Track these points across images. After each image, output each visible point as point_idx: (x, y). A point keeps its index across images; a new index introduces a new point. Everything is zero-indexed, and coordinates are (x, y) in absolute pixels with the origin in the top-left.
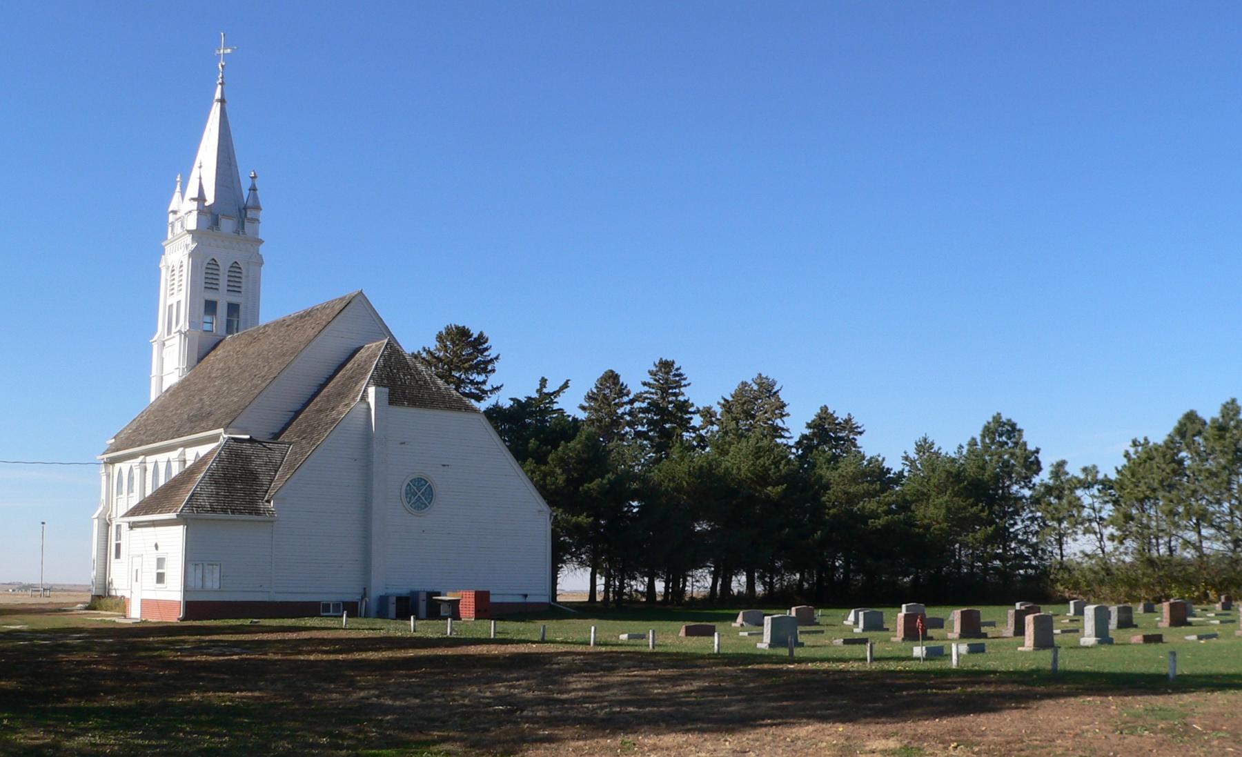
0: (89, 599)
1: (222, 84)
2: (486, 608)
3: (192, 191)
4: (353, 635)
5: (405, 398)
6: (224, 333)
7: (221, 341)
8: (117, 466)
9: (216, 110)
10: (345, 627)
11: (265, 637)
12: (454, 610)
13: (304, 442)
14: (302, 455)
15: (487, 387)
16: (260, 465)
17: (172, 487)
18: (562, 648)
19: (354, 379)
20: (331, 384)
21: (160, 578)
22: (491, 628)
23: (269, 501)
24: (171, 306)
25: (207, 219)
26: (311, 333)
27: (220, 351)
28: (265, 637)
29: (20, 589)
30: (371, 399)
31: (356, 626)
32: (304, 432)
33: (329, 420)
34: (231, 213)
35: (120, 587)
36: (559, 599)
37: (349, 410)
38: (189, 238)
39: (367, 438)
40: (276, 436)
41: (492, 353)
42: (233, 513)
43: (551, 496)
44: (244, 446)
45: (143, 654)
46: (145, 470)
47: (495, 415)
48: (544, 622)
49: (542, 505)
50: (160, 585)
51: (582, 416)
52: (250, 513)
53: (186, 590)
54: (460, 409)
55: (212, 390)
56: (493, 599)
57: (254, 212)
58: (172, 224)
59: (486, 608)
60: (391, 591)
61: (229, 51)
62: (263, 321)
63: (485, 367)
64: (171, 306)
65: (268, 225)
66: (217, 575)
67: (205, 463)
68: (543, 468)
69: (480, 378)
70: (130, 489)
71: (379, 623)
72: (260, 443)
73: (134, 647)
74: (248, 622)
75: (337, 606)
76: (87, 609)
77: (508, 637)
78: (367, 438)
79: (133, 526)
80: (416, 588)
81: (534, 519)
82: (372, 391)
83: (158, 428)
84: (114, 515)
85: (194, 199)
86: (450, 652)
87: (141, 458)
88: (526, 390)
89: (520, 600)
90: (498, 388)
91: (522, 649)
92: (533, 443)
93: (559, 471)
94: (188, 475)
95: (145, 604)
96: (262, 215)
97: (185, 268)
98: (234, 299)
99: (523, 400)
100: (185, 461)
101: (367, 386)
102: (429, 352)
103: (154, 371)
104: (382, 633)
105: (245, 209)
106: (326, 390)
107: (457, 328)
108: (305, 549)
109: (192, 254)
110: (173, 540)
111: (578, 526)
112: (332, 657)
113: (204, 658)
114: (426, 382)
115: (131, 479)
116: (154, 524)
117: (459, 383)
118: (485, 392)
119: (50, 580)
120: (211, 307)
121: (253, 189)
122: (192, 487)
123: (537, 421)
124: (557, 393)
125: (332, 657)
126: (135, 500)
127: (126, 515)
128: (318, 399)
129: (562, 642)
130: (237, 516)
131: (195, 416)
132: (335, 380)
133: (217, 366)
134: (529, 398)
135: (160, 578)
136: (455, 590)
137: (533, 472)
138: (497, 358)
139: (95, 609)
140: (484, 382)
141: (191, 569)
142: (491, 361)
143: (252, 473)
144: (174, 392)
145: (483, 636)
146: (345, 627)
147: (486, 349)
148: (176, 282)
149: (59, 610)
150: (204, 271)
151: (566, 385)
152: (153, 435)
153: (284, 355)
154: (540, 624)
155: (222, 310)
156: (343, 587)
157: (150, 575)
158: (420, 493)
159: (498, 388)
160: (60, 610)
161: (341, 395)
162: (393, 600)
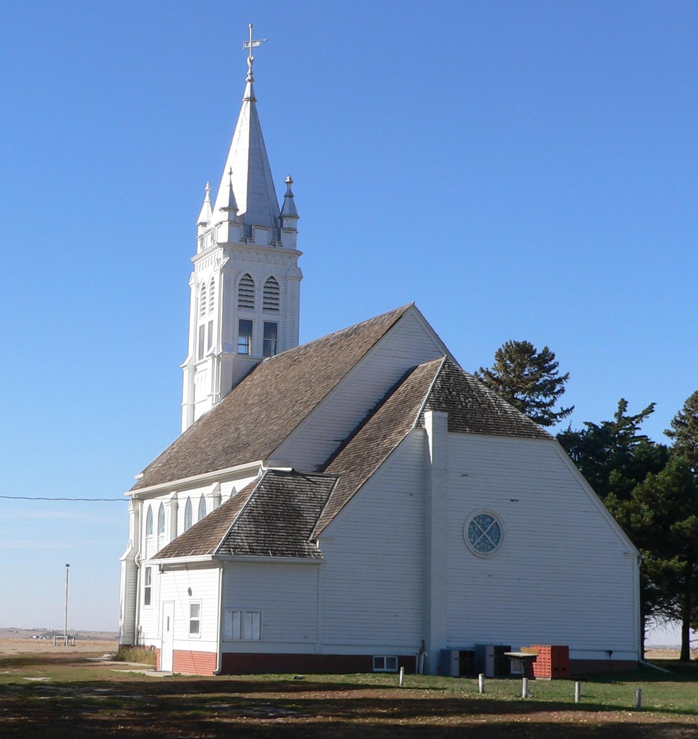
0: (116, 649)
1: (251, 80)
2: (564, 666)
3: (223, 200)
4: (412, 695)
5: (467, 423)
6: (261, 355)
7: (257, 365)
8: (147, 503)
9: (246, 109)
10: (402, 686)
11: (312, 695)
12: (528, 665)
13: (352, 474)
14: (351, 489)
15: (555, 410)
16: (304, 501)
17: (206, 526)
18: (665, 719)
19: (408, 403)
20: (382, 410)
21: (194, 627)
22: (575, 690)
23: (314, 542)
24: (202, 327)
25: (240, 232)
26: (358, 352)
27: (256, 376)
28: (312, 695)
29: (44, 635)
30: (428, 425)
31: (415, 684)
32: (353, 463)
33: (380, 449)
34: (266, 224)
35: (149, 637)
36: (647, 656)
37: (405, 438)
38: (220, 252)
39: (425, 469)
40: (321, 468)
41: (561, 372)
42: (274, 554)
43: (638, 536)
44: (286, 479)
45: (175, 713)
46: (177, 507)
47: (567, 440)
48: (642, 685)
49: (631, 548)
50: (194, 635)
51: (670, 443)
52: (294, 555)
53: (223, 640)
54: (530, 436)
55: (248, 418)
56: (573, 656)
57: (291, 220)
58: (202, 237)
59: (564, 666)
60: (453, 644)
61: (258, 44)
62: (303, 341)
63: (552, 388)
64: (202, 327)
65: (306, 235)
66: (257, 624)
67: (243, 499)
68: (626, 503)
69: (547, 400)
70: (161, 528)
71: (441, 681)
72: (304, 476)
73: (165, 706)
74: (291, 677)
75: (391, 660)
76: (115, 659)
77: (594, 701)
78: (425, 469)
79: (163, 569)
80: (482, 641)
81: (618, 561)
82: (428, 416)
83: (191, 460)
84: (143, 557)
85: (224, 209)
86: (528, 718)
87: (172, 494)
88: (603, 414)
89: (604, 657)
90: (568, 411)
91: (616, 717)
92: (614, 475)
93: (645, 507)
94: (224, 512)
95: (178, 655)
96: (300, 225)
97: (216, 285)
98: (271, 317)
99: (600, 426)
100: (220, 497)
101: (423, 410)
102: (488, 374)
103: (186, 398)
104: (446, 695)
105: (281, 218)
106: (376, 416)
107: (517, 345)
108: (357, 593)
109: (224, 270)
110: (208, 584)
111: (668, 571)
112: (390, 721)
113: (244, 720)
114: (490, 405)
115: (161, 517)
116: (187, 566)
117: (524, 406)
118: (554, 416)
119: (75, 625)
120: (245, 327)
121: (289, 195)
122: (229, 525)
123: (616, 449)
124: (639, 418)
125: (390, 721)
126: (166, 540)
127: (157, 557)
128: (367, 426)
129: (662, 710)
130: (279, 558)
131: (232, 447)
132: (386, 405)
133: (253, 391)
134: (607, 423)
135: (194, 627)
136: (528, 645)
137: (614, 508)
138: (566, 377)
139: (122, 660)
140: (552, 403)
141: (228, 616)
142: (560, 381)
143: (294, 509)
144: (207, 422)
145: (567, 700)
146: (402, 686)
147: (554, 367)
148: (207, 300)
149: (82, 660)
150: (238, 287)
151: (650, 410)
152: (185, 468)
153: (329, 377)
154: (633, 687)
155: (258, 330)
156: (399, 640)
157: (183, 624)
158: (486, 533)
159: (568, 411)
160: (86, 661)
161: (394, 421)
162: (456, 655)
